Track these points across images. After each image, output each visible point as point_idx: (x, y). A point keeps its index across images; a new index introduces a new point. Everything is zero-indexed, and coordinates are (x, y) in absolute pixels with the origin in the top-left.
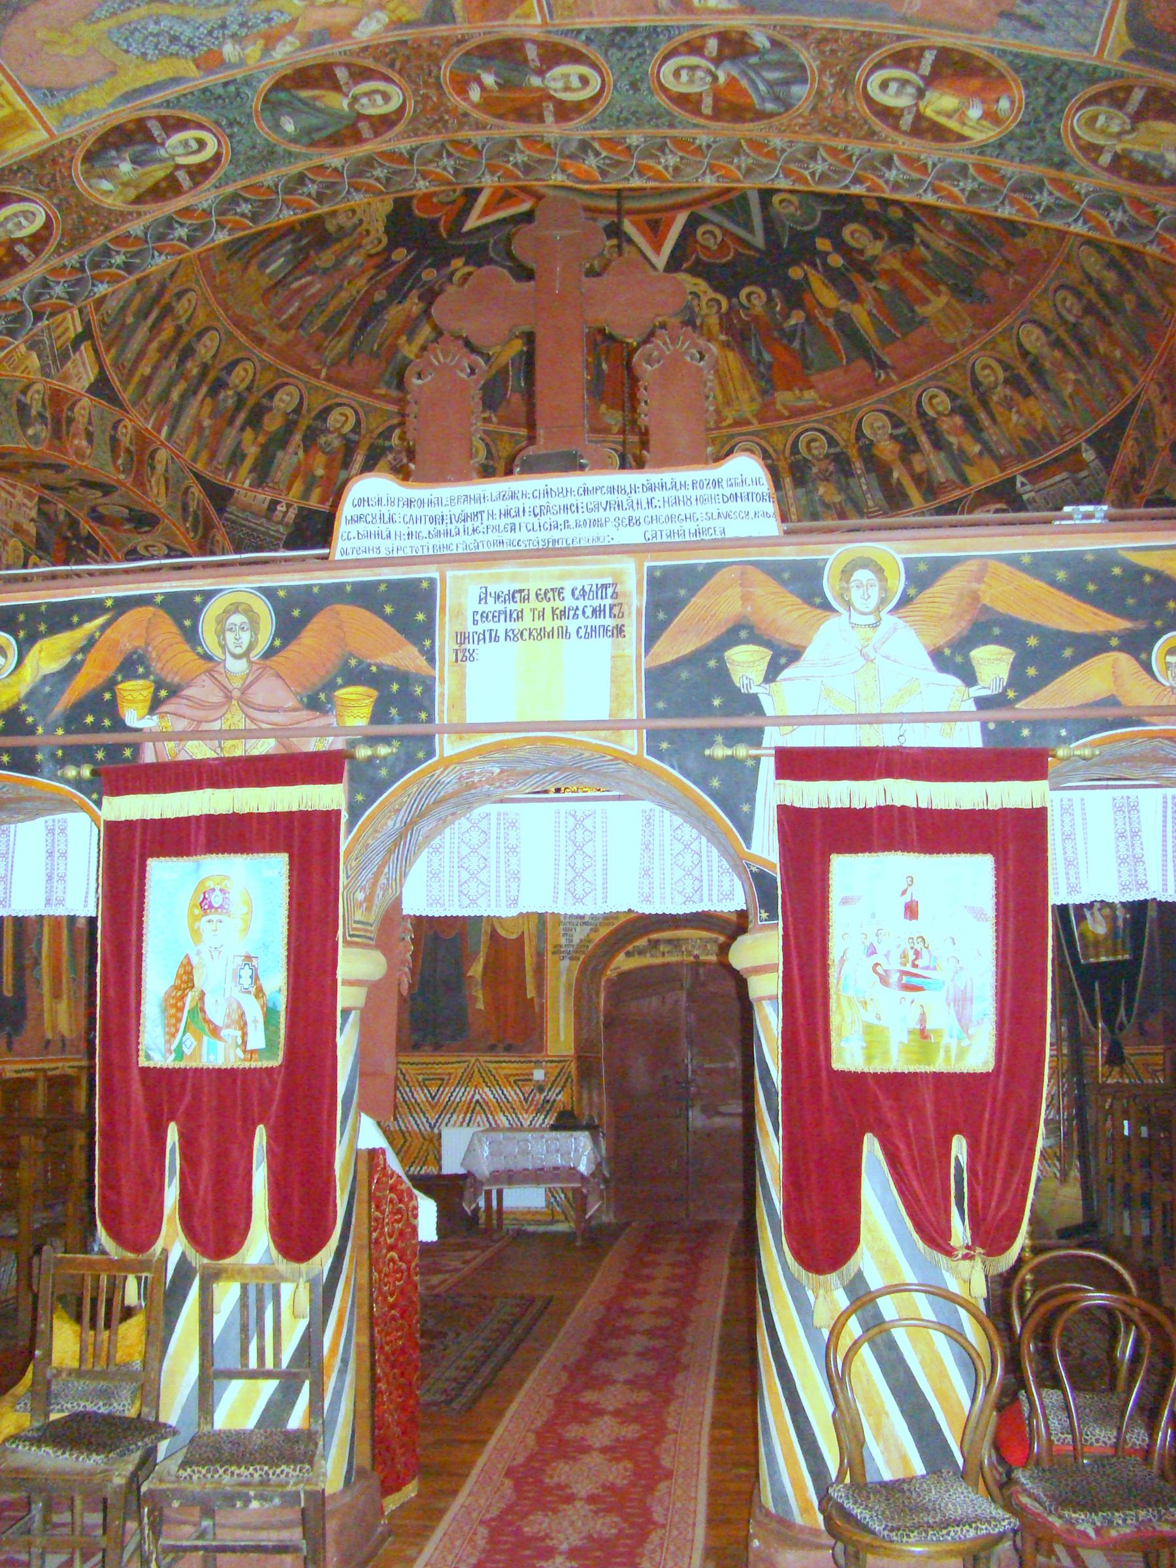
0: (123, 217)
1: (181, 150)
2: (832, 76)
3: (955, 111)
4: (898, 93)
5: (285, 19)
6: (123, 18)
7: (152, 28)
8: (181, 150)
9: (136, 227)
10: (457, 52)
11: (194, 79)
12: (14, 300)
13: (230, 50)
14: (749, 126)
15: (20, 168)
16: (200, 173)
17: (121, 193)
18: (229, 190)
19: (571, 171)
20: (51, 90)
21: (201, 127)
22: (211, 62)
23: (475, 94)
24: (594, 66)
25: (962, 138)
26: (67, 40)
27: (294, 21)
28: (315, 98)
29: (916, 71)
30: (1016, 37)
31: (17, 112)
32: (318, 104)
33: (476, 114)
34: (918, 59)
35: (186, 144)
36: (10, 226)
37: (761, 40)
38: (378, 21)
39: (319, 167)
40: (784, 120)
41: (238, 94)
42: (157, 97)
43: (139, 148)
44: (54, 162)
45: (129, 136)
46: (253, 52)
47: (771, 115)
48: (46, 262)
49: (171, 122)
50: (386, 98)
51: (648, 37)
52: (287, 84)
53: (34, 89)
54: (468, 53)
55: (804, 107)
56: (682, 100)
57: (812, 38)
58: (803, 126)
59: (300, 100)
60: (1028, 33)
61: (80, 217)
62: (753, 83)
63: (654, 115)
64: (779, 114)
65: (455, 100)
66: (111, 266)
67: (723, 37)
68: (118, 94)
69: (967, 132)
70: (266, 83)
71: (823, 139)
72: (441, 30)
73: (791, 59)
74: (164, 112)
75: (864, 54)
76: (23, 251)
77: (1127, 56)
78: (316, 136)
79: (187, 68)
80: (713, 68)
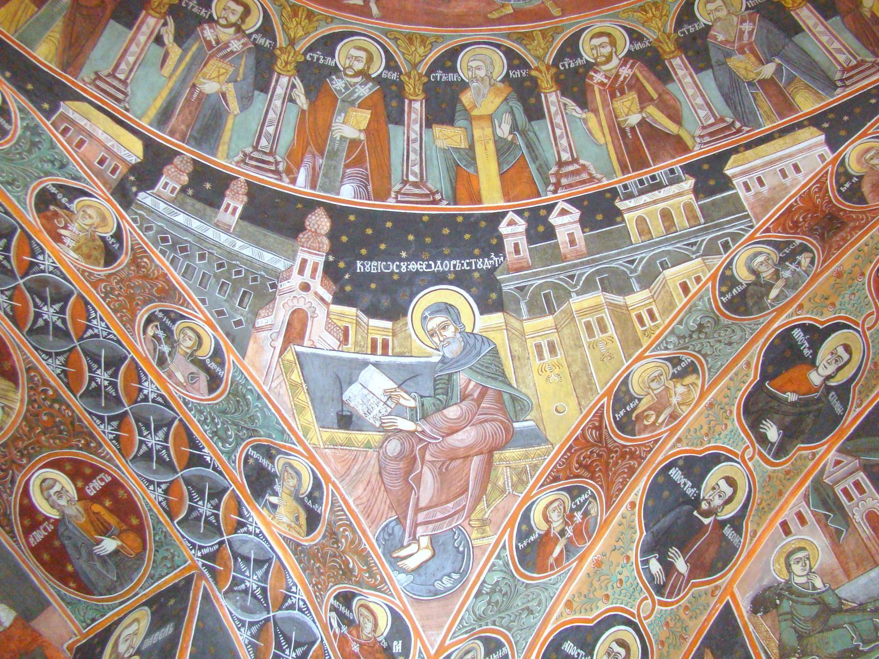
0: (38, 386)
36: (63, 502)
48: (110, 460)
76: (96, 485)
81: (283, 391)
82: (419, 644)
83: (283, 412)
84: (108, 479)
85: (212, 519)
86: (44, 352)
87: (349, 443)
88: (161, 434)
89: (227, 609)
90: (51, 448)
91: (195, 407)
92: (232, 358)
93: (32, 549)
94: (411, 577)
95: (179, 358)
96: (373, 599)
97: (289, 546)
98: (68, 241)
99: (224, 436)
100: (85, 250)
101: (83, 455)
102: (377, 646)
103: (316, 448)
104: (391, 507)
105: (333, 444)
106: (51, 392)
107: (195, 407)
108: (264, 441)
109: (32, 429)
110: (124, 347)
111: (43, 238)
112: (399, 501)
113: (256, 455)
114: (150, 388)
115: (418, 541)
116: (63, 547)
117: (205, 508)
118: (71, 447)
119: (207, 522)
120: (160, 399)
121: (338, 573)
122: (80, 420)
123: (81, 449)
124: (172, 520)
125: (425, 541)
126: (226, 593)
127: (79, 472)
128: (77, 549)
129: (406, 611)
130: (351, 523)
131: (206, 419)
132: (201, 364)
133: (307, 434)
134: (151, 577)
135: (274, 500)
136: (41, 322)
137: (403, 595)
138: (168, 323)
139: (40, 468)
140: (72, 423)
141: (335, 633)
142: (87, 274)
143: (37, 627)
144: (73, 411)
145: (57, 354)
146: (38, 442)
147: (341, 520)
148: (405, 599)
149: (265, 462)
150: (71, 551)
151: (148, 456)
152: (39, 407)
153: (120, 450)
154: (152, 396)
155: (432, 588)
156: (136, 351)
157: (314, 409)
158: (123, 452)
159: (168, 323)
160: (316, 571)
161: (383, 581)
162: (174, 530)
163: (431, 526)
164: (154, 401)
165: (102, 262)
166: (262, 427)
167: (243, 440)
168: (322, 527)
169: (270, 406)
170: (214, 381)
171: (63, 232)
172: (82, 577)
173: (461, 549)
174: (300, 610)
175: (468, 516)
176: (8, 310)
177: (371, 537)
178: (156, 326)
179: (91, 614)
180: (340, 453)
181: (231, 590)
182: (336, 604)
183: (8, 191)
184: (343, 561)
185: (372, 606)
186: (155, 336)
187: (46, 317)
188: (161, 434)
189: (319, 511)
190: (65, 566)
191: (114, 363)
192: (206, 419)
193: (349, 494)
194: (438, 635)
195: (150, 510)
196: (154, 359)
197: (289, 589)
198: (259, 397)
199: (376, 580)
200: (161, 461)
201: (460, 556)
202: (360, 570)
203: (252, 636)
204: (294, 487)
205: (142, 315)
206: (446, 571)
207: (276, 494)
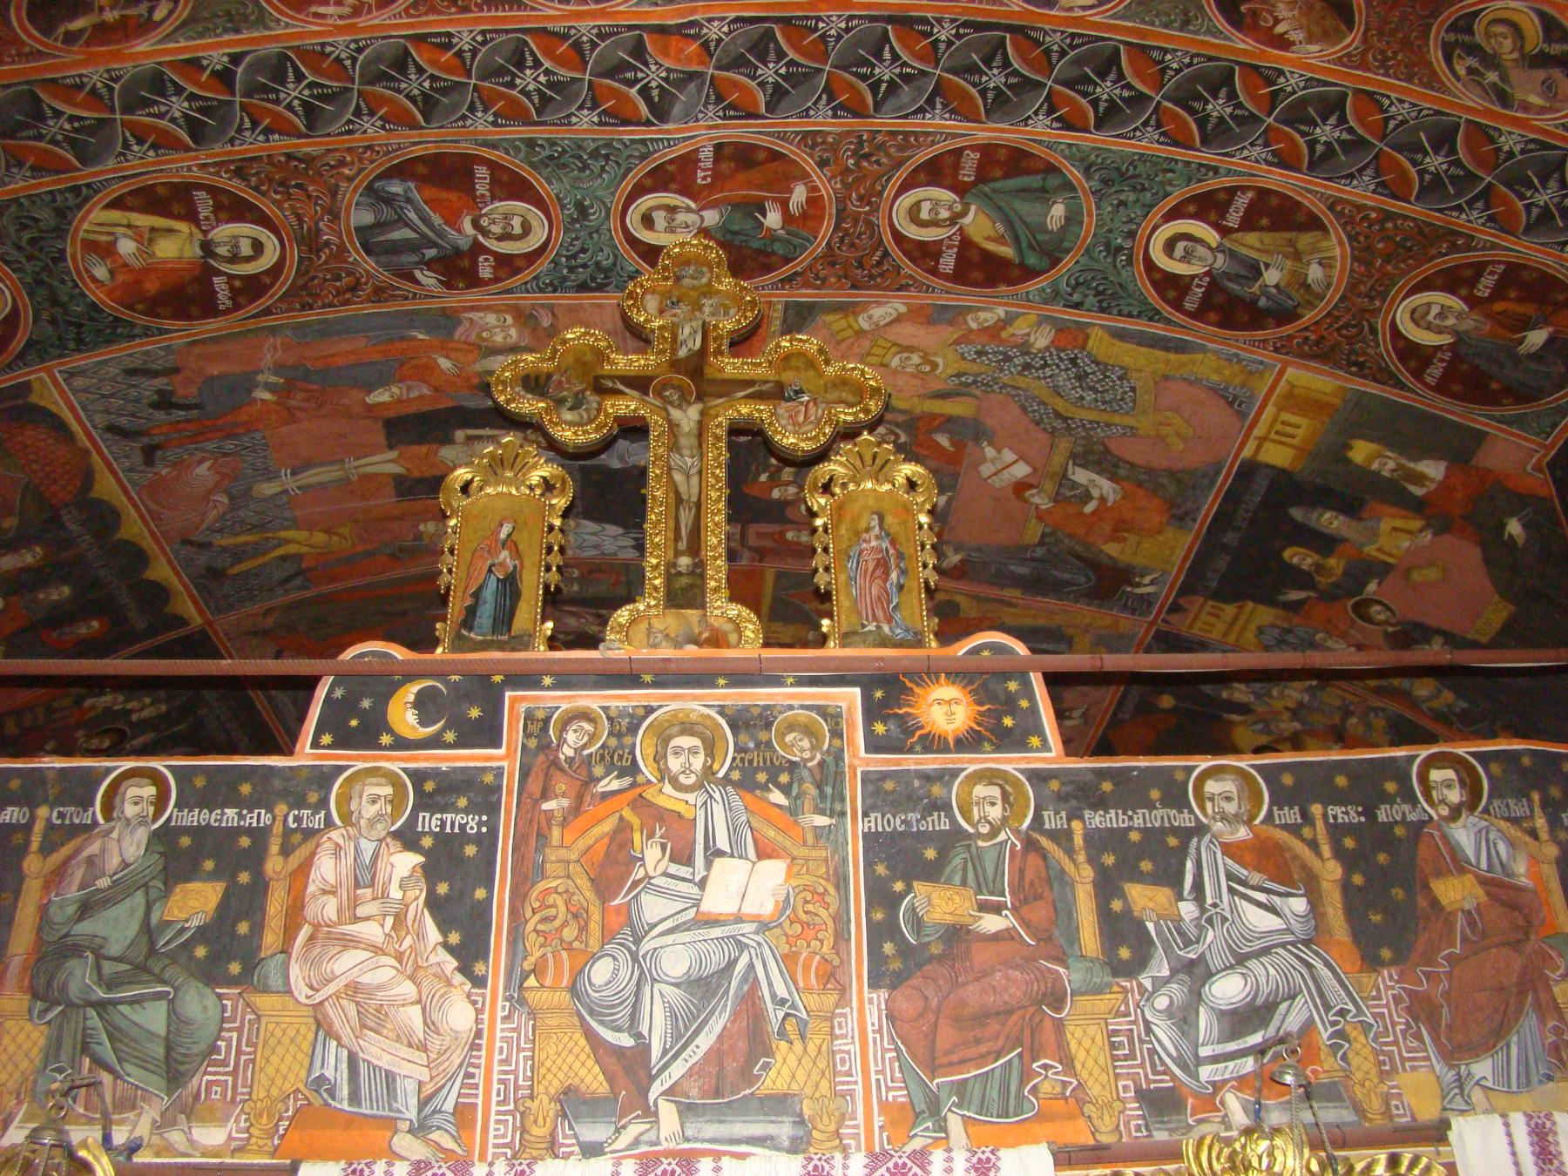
2: (327, 244)
3: (151, 241)
4: (234, 242)
5: (963, 348)
6: (1105, 418)
7: (1089, 396)
10: (801, 262)
14: (418, 151)
15: (1351, 364)
18: (1207, 156)
19: (694, 47)
20: (1231, 404)
23: (799, 195)
24: (633, 242)
25: (117, 204)
26: (1165, 430)
27: (957, 342)
28: (999, 240)
29: (231, 277)
30: (147, 353)
32: (1000, 228)
33: (808, 163)
34: (235, 293)
36: (1451, 321)
37: (428, 279)
38: (870, 318)
40: (373, 170)
42: (1158, 329)
45: (1229, 305)
46: (1020, 328)
47: (388, 174)
48: (1494, 246)
50: (913, 214)
51: (564, 279)
52: (1016, 272)
54: (787, 260)
55: (350, 194)
56: (516, 188)
57: (369, 289)
58: (342, 163)
60: (137, 364)
62: (426, 220)
63: (555, 162)
64: (379, 177)
65: (826, 190)
67: (474, 281)
68: (1184, 358)
69: (115, 215)
71: (308, 147)
73: (383, 259)
74: (1166, 310)
75: (300, 282)
77: (26, 387)
78: (1034, 181)
79: (1099, 343)
80: (480, 238)
90: (1404, 273)
95: (1515, 75)
98: (1293, 36)
109: (1368, 264)
110: (1448, 115)
111: (1273, 57)
114: (1510, 140)
118: (1433, 258)
120: (1532, 146)
136: (1320, 148)
139: (1403, 299)
140: (1421, 233)
143: (1480, 465)
144: (1414, 219)
145: (1360, 171)
152: (1367, 238)
153: (1501, 230)
154: (1517, 149)
158: (1508, 230)
159: (1466, 38)
164: (1522, 152)
165: (1343, 27)
171: (1280, 29)
176: (1270, 158)
186: (1471, 71)
187: (1323, 139)
191: (1444, 138)
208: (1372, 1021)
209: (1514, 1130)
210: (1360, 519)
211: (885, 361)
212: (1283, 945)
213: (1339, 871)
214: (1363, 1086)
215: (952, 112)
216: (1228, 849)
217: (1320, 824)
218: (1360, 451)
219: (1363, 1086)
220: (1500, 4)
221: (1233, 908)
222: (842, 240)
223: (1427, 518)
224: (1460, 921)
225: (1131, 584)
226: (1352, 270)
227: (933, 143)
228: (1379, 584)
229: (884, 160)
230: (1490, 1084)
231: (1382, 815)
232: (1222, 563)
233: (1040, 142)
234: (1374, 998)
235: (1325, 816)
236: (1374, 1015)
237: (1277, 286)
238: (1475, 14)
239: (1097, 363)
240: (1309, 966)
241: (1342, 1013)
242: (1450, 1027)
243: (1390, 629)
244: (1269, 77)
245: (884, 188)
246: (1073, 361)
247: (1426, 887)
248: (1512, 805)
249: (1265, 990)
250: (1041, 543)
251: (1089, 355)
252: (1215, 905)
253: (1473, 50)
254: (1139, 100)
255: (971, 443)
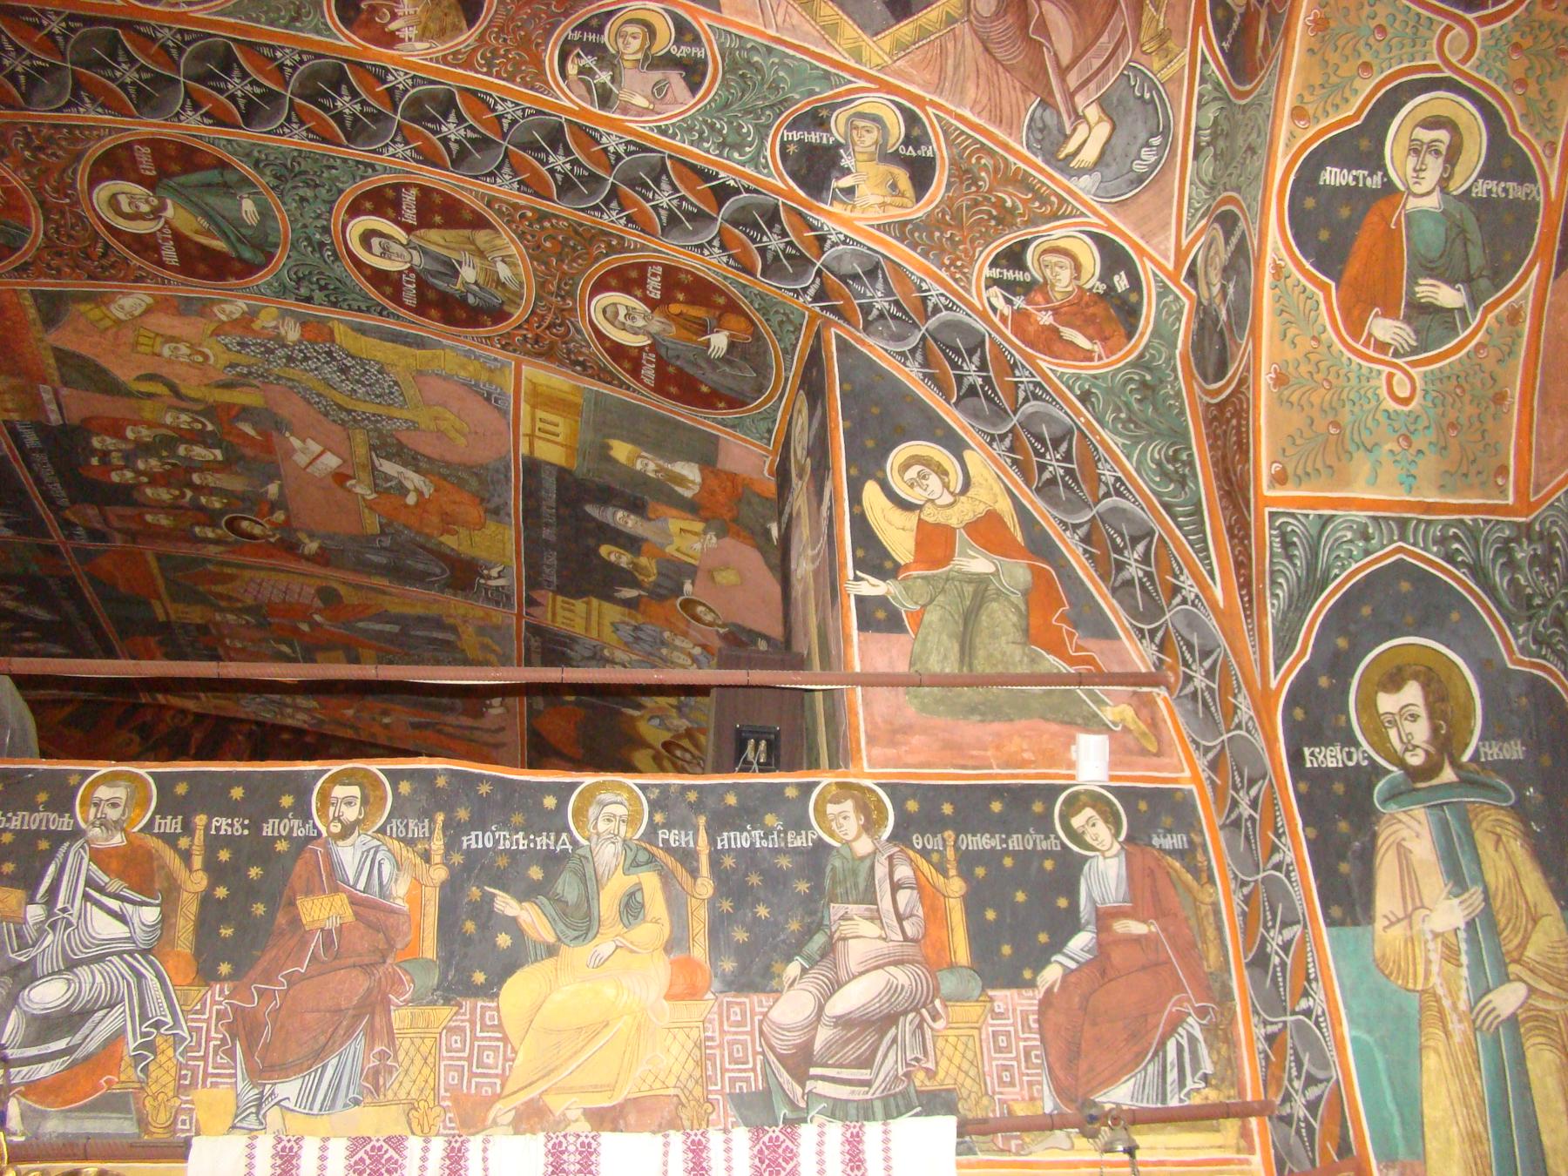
0: (513, 215)
1: (389, 246)
7: (361, 391)
8: (389, 246)
9: (506, 188)
10: (27, 251)
11: (341, 321)
12: (723, 247)
13: (292, 333)
16: (383, 201)
17: (496, 248)
18: (357, 153)
20: (488, 399)
21: (358, 263)
22: (316, 331)
26: (444, 425)
27: (215, 333)
28: (207, 233)
31: (534, 407)
35: (385, 253)
36: (640, 323)
38: (122, 308)
39: (219, 123)
41: (299, 280)
42: (390, 325)
43: (440, 284)
44: (537, 340)
48: (644, 248)
49: (388, 290)
50: (113, 202)
52: (238, 266)
53: (505, 413)
59: (228, 238)
61: (561, 260)
66: (575, 162)
70: (262, 279)
72: (48, 285)
76: (654, 286)
78: (212, 176)
81: (796, 19)
82: (1149, 264)
83: (812, 48)
84: (659, 270)
85: (789, 250)
86: (486, 175)
87: (923, 33)
88: (665, 186)
89: (876, 349)
91: (680, 128)
92: (704, 21)
93: (654, 390)
94: (1097, 176)
95: (630, 75)
96: (1057, 233)
97: (889, 234)
98: (405, 34)
99: (738, 140)
100: (433, 26)
101: (616, 260)
102: (1086, 298)
103: (882, 69)
104: (1026, 90)
105: (901, 47)
106: (529, 214)
107: (680, 128)
108: (802, 106)
109: (547, 264)
111: (378, 54)
112: (1031, 75)
113: (796, 136)
115: (1084, 117)
116: (679, 369)
117: (774, 243)
118: (597, 259)
119: (788, 257)
120: (632, 148)
121: (987, 227)
122: (581, 225)
123: (607, 255)
124: (753, 274)
125: (1093, 113)
126: (865, 329)
127: (628, 279)
128: (696, 365)
129: (1111, 227)
130: (983, 144)
131: (701, 133)
132: (669, 61)
133: (860, 56)
134: (785, 351)
135: (846, 182)
137: (1097, 206)
138: (592, 37)
140: (576, 232)
141: (1002, 315)
142: (450, 58)
144: (566, 219)
145: (499, 168)
146: (564, 273)
147: (967, 147)
148: (1102, 211)
149: (814, 137)
150: (691, 370)
151: (673, 220)
154: (621, 149)
155: (1132, 176)
156: (564, 109)
157: (850, 16)
158: (646, 230)
159: (592, 37)
160: (947, 245)
161: (1062, 200)
162: (768, 286)
163: (1092, 86)
165: (464, 24)
166: (794, 88)
167: (769, 127)
168: (942, 173)
169: (791, 52)
170: (693, 72)
172: (723, 391)
173: (1147, 96)
174: (946, 308)
175: (1137, 40)
177: (1019, 150)
178: (578, 55)
179: (763, 426)
180: (918, 56)
181: (867, 324)
182: (995, 273)
183: (301, 30)
184: (994, 205)
185: (1062, 244)
188: (665, 186)
189: (930, 154)
190: (698, 391)
191: (555, 138)
192: (701, 133)
193: (960, 105)
194: (1167, 239)
195: (726, 278)
196: (592, 104)
197: (920, 289)
198: (769, 50)
199: (1052, 204)
200: (691, 217)
201: (1150, 107)
202: (1024, 202)
203: (922, 366)
204: (876, 143)
205: (551, 56)
206: (1141, 140)
207: (846, 172)
208: (186, 1035)
209: (670, 1158)
210: (649, 519)
211: (157, 350)
212: (120, 954)
213: (205, 883)
214: (155, 1099)
215: (103, 106)
216: (98, 857)
217: (199, 835)
218: (621, 451)
219: (155, 1099)
220: (639, 4)
221: (82, 915)
222: (57, 231)
223: (706, 520)
224: (316, 941)
225: (482, 576)
226: (535, 270)
227: (100, 138)
228: (693, 584)
229: (60, 153)
230: (291, 1106)
231: (267, 830)
232: (551, 559)
233: (201, 138)
234: (196, 1012)
235: (207, 827)
236: (190, 1029)
237: (476, 283)
238: (610, 14)
239: (353, 358)
240: (139, 976)
241: (158, 1025)
242: (267, 1046)
243: (721, 631)
244: (380, 75)
245: (74, 180)
246: (329, 353)
247: (292, 903)
248: (411, 826)
249: (86, 996)
250: (383, 533)
251: (341, 348)
252: (64, 910)
253: (598, 50)
254: (271, 97)
255: (275, 434)
